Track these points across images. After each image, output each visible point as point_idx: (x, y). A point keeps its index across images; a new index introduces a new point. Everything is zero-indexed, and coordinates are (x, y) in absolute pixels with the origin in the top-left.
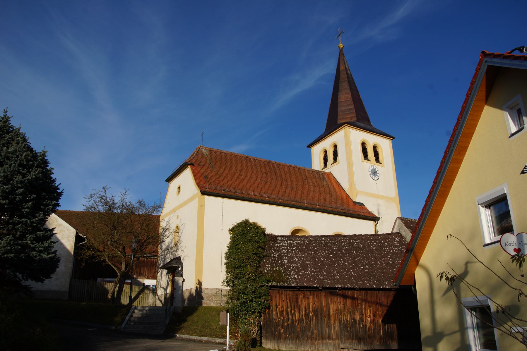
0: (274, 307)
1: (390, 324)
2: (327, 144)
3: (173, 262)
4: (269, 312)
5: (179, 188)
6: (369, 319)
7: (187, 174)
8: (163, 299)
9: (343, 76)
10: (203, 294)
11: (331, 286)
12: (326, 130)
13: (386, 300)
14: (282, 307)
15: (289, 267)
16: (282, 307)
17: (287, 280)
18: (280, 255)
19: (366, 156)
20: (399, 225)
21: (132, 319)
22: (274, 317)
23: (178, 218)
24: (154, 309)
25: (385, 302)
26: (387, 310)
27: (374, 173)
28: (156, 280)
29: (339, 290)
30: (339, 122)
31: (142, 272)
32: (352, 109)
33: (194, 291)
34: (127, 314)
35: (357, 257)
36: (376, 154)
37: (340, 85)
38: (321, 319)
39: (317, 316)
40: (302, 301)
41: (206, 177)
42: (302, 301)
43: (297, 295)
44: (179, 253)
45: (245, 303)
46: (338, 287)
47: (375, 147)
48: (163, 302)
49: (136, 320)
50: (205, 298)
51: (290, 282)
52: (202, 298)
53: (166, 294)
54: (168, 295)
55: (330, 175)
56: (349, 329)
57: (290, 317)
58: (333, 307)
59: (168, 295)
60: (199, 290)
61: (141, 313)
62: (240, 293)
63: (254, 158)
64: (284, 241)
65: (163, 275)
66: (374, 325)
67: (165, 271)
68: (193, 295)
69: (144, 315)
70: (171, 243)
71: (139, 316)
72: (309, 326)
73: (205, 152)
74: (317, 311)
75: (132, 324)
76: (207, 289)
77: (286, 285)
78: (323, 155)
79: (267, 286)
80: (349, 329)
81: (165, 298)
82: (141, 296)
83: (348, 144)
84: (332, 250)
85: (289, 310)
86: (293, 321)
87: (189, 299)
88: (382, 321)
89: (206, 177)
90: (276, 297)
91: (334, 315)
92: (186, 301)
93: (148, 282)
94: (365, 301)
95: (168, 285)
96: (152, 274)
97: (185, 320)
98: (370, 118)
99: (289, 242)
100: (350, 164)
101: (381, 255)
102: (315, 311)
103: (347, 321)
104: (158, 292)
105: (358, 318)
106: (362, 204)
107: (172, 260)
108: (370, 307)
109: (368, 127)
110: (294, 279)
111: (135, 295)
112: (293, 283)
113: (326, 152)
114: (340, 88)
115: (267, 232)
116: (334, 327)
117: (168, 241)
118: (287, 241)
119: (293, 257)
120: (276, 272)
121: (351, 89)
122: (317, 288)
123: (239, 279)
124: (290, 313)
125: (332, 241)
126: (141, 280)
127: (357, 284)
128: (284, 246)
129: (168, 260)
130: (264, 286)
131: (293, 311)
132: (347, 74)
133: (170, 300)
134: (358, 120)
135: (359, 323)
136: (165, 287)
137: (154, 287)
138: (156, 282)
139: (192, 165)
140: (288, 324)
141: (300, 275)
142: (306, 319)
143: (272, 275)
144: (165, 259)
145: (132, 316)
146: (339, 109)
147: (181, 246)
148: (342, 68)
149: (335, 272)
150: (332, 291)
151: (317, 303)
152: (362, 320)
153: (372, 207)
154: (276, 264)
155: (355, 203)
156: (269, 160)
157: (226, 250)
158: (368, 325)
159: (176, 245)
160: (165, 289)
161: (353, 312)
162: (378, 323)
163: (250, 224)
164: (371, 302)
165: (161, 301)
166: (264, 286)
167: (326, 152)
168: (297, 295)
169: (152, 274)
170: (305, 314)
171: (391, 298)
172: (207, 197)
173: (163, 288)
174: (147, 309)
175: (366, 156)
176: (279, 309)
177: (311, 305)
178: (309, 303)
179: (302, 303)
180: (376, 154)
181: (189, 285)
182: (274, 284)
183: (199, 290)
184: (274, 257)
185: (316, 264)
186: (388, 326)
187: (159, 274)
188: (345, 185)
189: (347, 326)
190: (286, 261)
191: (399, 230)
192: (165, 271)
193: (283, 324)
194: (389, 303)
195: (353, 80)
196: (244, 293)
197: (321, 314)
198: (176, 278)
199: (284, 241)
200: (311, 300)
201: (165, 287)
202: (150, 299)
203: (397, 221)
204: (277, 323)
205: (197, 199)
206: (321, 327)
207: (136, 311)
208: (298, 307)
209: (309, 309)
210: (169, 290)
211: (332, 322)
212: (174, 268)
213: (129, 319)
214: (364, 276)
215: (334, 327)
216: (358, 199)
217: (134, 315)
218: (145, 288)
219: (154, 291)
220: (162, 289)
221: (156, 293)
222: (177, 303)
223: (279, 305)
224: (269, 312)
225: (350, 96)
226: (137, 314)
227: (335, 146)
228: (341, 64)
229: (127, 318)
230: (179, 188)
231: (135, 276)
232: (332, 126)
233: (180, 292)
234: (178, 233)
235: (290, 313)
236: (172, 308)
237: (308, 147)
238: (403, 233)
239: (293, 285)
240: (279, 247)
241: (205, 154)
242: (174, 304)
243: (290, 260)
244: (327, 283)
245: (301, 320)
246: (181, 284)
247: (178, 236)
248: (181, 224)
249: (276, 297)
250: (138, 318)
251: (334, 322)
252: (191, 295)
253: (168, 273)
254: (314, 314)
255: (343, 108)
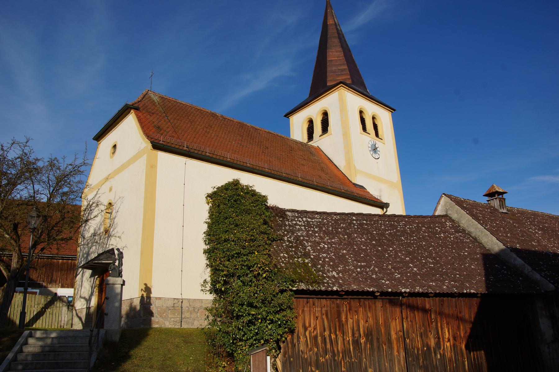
0: (301, 330)
1: (476, 351)
2: (313, 111)
3: (101, 257)
4: (292, 339)
5: (115, 146)
6: (448, 344)
7: (131, 122)
8: (83, 315)
9: (332, 31)
10: (153, 308)
11: (394, 291)
12: (311, 94)
13: (469, 311)
14: (315, 329)
15: (317, 258)
16: (315, 329)
17: (322, 280)
18: (297, 238)
19: (364, 129)
20: (445, 205)
21: (20, 357)
22: (301, 348)
23: (111, 190)
24: (66, 336)
25: (467, 317)
26: (471, 329)
27: (375, 149)
28: (73, 289)
29: (403, 297)
30: (329, 84)
31: (54, 278)
32: (345, 69)
33: (137, 303)
34: (10, 348)
35: (410, 245)
36: (375, 127)
37: (329, 41)
38: (379, 348)
39: (372, 344)
40: (346, 318)
41: (159, 127)
42: (346, 318)
43: (338, 306)
44: (113, 243)
45: (250, 323)
46: (405, 292)
47: (374, 118)
48: (83, 319)
49: (29, 358)
50: (155, 314)
51: (328, 283)
52: (151, 314)
53: (88, 308)
54: (92, 310)
55: (318, 149)
56: (421, 364)
57: (328, 346)
58: (395, 326)
59: (92, 310)
60: (146, 301)
61: (40, 343)
62: (242, 305)
63: (222, 116)
64: (297, 217)
65: (84, 279)
66: (455, 355)
67: (88, 272)
68: (135, 308)
69: (47, 349)
70: (99, 229)
71: (37, 350)
72: (360, 362)
73: (156, 99)
74: (371, 334)
75: (20, 367)
76: (160, 298)
77: (323, 289)
78: (306, 126)
79: (291, 290)
80: (421, 364)
81: (88, 315)
82: (48, 310)
83: (343, 109)
84: (372, 234)
85: (327, 333)
86: (334, 355)
87: (128, 315)
88: (467, 347)
89: (159, 127)
90: (303, 311)
91: (398, 340)
92: (123, 319)
93: (62, 292)
94: (441, 314)
95: (92, 294)
96: (69, 281)
97: (127, 357)
98: (365, 83)
99: (304, 219)
100: (346, 135)
101: (438, 243)
102: (368, 334)
103: (418, 351)
104: (76, 305)
105: (432, 343)
106: (362, 187)
107: (99, 255)
108: (448, 324)
109: (365, 93)
110: (333, 278)
111: (39, 309)
112: (334, 285)
113: (311, 122)
114: (328, 45)
115: (271, 202)
116: (399, 361)
117: (92, 226)
118: (302, 218)
119: (319, 243)
120: (299, 265)
121: (342, 47)
122: (373, 292)
123: (239, 277)
124: (328, 341)
125: (367, 221)
126: (53, 290)
127: (430, 286)
128: (300, 226)
129: (93, 256)
130: (285, 291)
131: (333, 336)
132: (337, 29)
133: (97, 317)
134: (353, 82)
135: (435, 353)
136: (87, 297)
137: (70, 299)
138: (73, 292)
139: (137, 109)
140: (326, 360)
141: (340, 272)
142: (354, 349)
143: (295, 272)
144: (88, 254)
145: (21, 351)
146: (329, 69)
147: (117, 231)
148: (330, 22)
149: (390, 267)
150: (392, 298)
151: (371, 320)
152: (438, 345)
153: (373, 190)
154: (296, 253)
155: (355, 184)
156: (242, 121)
157: (205, 228)
158: (448, 355)
159: (107, 231)
160: (88, 300)
161: (424, 335)
162: (461, 349)
163: (242, 189)
164: (448, 316)
165: (80, 319)
166: (285, 291)
167: (311, 122)
168: (338, 306)
169: (69, 281)
170: (353, 340)
171: (475, 309)
172: (162, 155)
173: (84, 298)
174: (54, 335)
175: (364, 129)
176: (310, 332)
177: (362, 323)
178: (358, 320)
179: (347, 321)
180: (375, 127)
181: (131, 293)
182: (303, 286)
183: (146, 301)
184: (288, 241)
185: (356, 254)
186: (474, 355)
187: (79, 277)
188: (339, 161)
189: (418, 359)
190: (309, 248)
191: (447, 212)
192: (88, 272)
193: (317, 360)
194: (473, 316)
195: (344, 37)
196: (251, 305)
197: (378, 339)
198: (111, 280)
199: (298, 217)
200: (361, 316)
201: (87, 297)
202: (63, 316)
203: (443, 199)
204: (306, 359)
205: (145, 156)
206: (379, 362)
207: (31, 341)
208: (342, 327)
209: (359, 330)
210: (94, 302)
211: (396, 353)
212: (105, 267)
213: (15, 359)
214: (434, 275)
215: (399, 361)
216: (358, 180)
217: (28, 349)
218: (56, 298)
219: (70, 304)
220: (82, 300)
221: (73, 306)
222: (111, 325)
223: (310, 326)
224: (292, 339)
225: (342, 54)
226: (33, 346)
227: (325, 114)
228: (329, 18)
229: (10, 355)
230: (115, 146)
231: (44, 284)
232: (319, 88)
233: (117, 304)
234: (111, 213)
235: (328, 341)
236: (102, 332)
237: (285, 116)
238: (454, 216)
239: (335, 289)
240: (292, 226)
241: (156, 101)
242: (106, 326)
243: (316, 246)
244: (387, 285)
245: (346, 352)
246: (118, 290)
247: (110, 218)
248: (117, 197)
249: (303, 311)
250: (34, 355)
251: (398, 351)
252: (132, 308)
253: (92, 276)
254: (367, 339)
255: (334, 68)
